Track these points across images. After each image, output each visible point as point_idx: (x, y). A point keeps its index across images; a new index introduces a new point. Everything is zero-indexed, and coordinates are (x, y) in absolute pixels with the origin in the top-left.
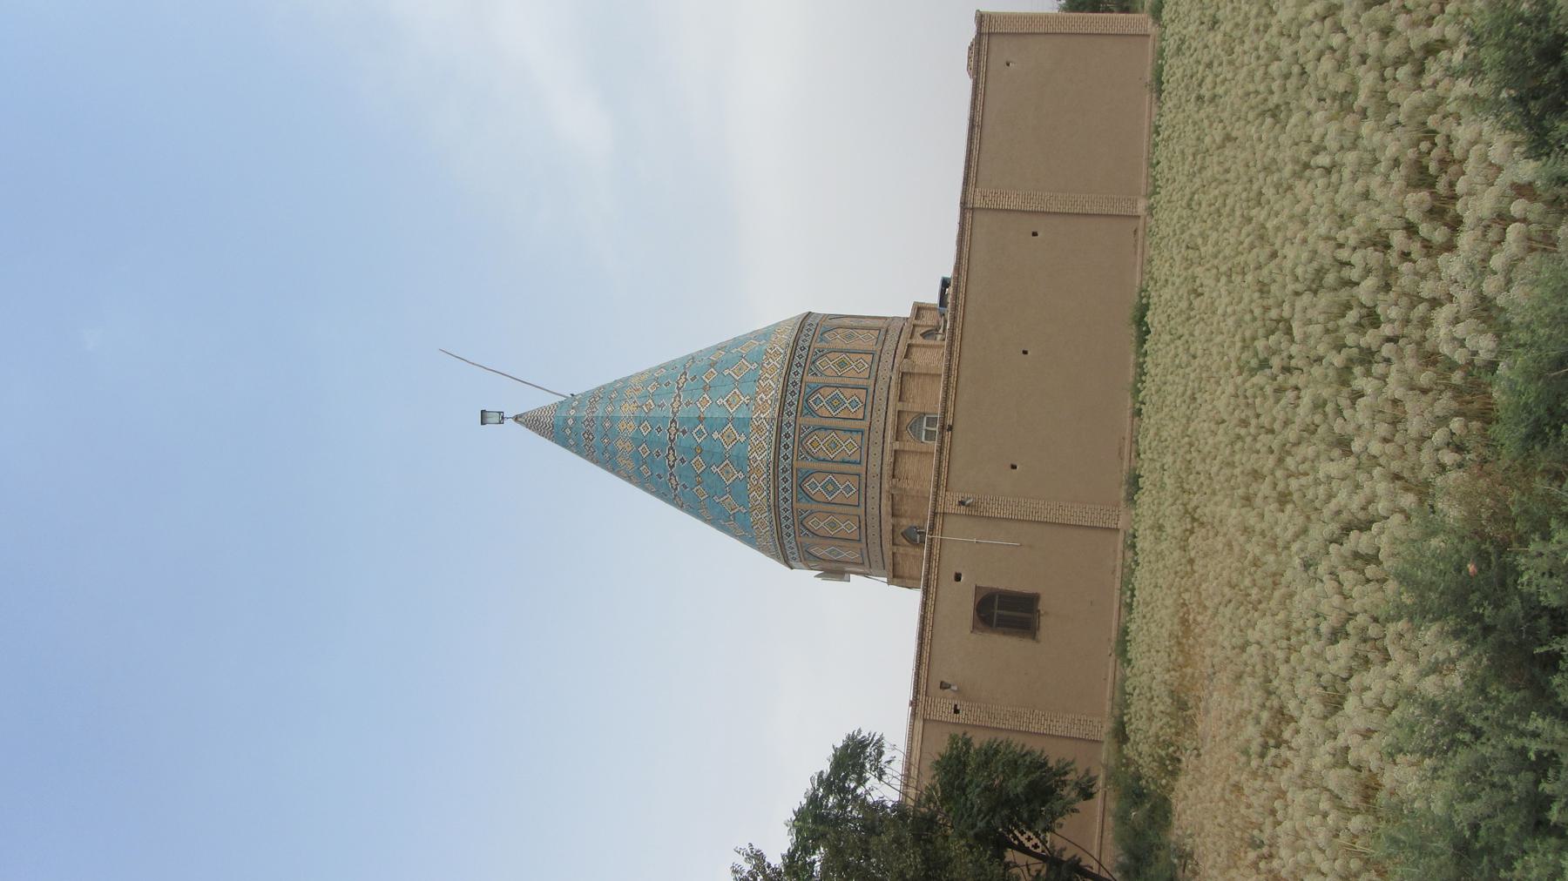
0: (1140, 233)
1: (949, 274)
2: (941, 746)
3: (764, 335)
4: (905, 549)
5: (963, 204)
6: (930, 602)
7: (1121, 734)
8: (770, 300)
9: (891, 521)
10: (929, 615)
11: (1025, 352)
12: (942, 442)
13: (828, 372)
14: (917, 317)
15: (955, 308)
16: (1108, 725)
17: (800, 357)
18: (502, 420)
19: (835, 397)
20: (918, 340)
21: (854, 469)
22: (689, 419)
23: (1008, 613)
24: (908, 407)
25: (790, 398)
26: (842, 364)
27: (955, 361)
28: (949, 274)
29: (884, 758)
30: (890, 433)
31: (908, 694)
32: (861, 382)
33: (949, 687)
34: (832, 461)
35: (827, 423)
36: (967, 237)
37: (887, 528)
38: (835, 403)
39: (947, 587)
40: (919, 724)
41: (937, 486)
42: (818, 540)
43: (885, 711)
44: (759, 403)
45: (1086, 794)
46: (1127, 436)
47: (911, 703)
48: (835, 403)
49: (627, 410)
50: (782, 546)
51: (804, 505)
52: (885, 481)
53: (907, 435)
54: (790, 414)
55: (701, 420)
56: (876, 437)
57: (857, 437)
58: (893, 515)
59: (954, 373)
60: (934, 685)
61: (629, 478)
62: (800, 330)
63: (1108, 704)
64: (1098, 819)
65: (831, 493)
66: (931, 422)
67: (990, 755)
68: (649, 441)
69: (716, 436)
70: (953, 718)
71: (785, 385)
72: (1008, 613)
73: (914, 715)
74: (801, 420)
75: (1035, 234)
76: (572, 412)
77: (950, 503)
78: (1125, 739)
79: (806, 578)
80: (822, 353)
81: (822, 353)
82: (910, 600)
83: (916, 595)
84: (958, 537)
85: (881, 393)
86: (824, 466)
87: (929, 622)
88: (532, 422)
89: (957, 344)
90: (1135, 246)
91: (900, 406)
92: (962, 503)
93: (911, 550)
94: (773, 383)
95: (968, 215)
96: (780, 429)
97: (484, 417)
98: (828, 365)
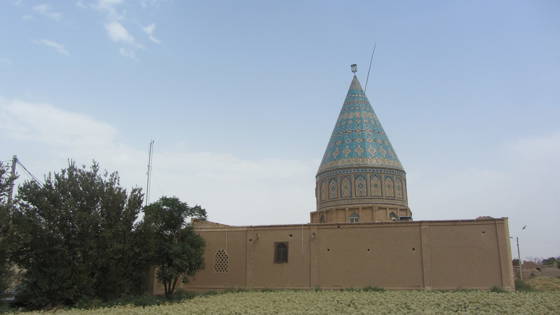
0: (418, 288)
5: (421, 222)
6: (282, 228)
11: (328, 250)
12: (334, 225)
17: (377, 171)
18: (354, 72)
19: (363, 185)
20: (389, 212)
21: (339, 196)
22: (353, 136)
24: (361, 211)
25: (360, 170)
26: (389, 186)
27: (362, 226)
30: (351, 206)
32: (369, 194)
34: (341, 188)
35: (353, 184)
38: (361, 186)
40: (246, 229)
48: (361, 186)
54: (354, 171)
56: (392, 202)
65: (332, 189)
66: (357, 220)
68: (354, 123)
69: (347, 147)
70: (248, 239)
73: (248, 227)
74: (353, 175)
75: (414, 249)
82: (416, 218)
85: (366, 201)
87: (276, 228)
88: (355, 82)
89: (369, 226)
90: (413, 287)
93: (318, 219)
95: (418, 224)
96: (349, 168)
97: (354, 66)
98: (388, 182)
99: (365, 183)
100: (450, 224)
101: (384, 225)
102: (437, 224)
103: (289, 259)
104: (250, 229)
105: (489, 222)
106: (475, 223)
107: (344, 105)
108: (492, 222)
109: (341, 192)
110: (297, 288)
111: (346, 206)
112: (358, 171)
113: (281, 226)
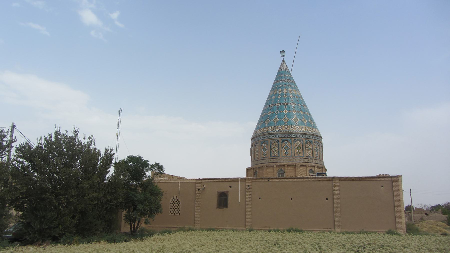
0: (330, 230)
5: (334, 178)
6: (223, 181)
10: (220, 181)
11: (260, 199)
13: (295, 145)
18: (283, 56)
20: (308, 169)
25: (286, 135)
26: (299, 148)
27: (287, 180)
30: (279, 164)
32: (293, 154)
35: (280, 146)
38: (286, 148)
40: (195, 181)
48: (286, 148)
53: (278, 168)
54: (282, 136)
58: (259, 168)
66: (283, 175)
69: (276, 116)
73: (197, 180)
74: (280, 139)
75: (327, 199)
87: (219, 181)
89: (292, 180)
90: (326, 229)
95: (331, 179)
96: (277, 134)
97: (283, 52)
98: (308, 145)
99: (290, 145)
100: (357, 179)
101: (305, 180)
103: (229, 205)
105: (387, 179)
108: (389, 179)
109: (271, 152)
112: (285, 136)
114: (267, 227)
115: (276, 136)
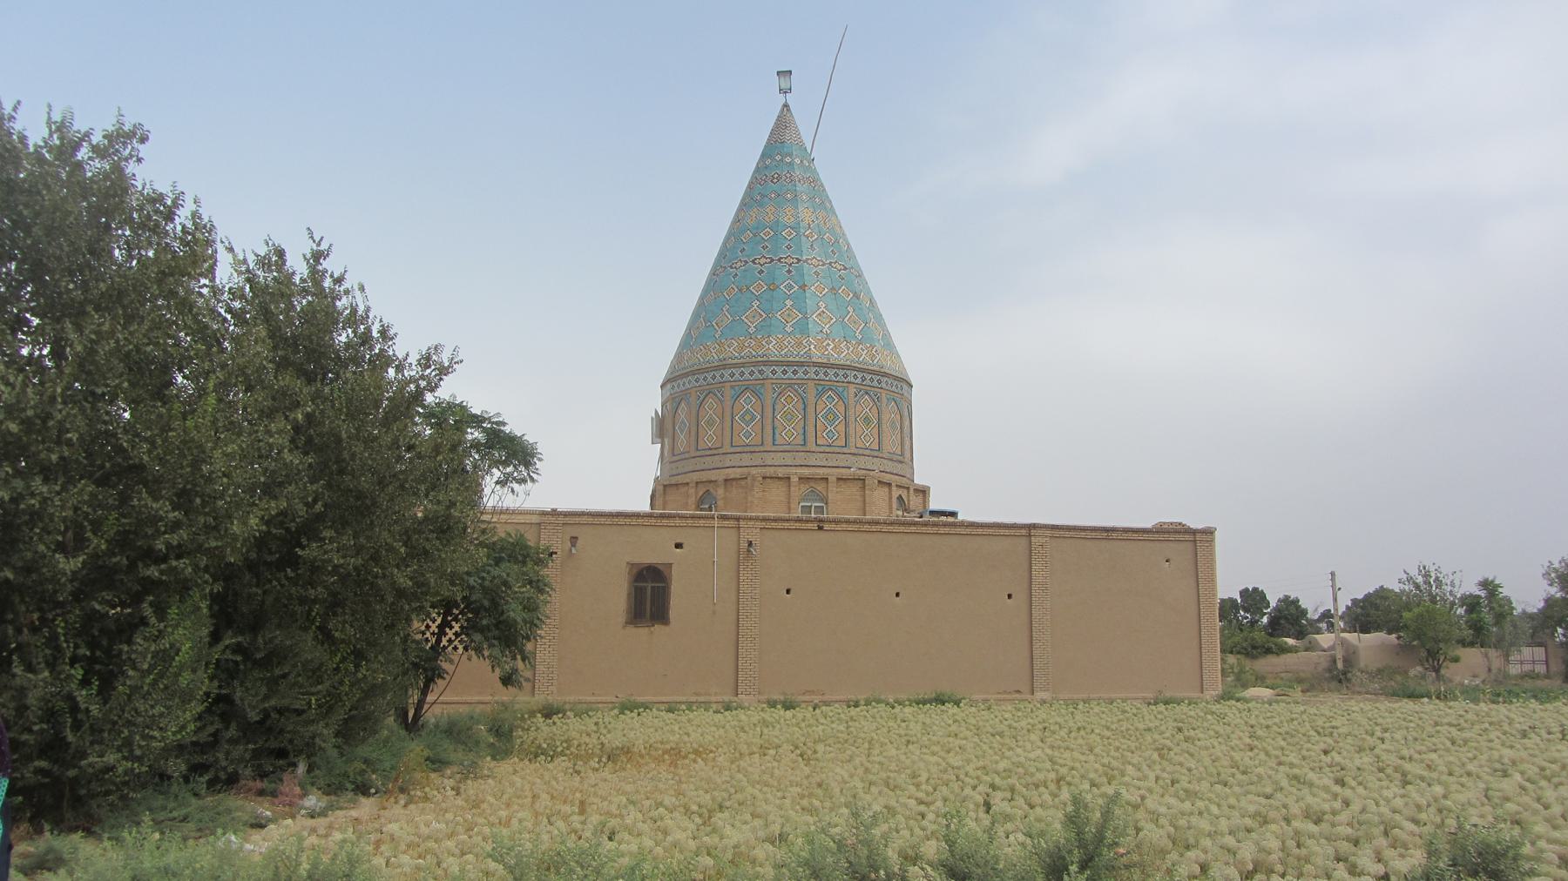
1: (960, 517)
2: (554, 540)
3: (889, 345)
4: (693, 495)
7: (549, 712)
8: (921, 346)
9: (721, 478)
11: (788, 592)
14: (916, 491)
15: (935, 525)
16: (555, 699)
17: (714, 377)
18: (785, 91)
20: (896, 493)
21: (768, 439)
23: (649, 595)
25: (831, 372)
26: (867, 420)
28: (960, 517)
29: (515, 486)
30: (806, 472)
31: (563, 505)
32: (852, 440)
33: (573, 545)
34: (774, 417)
35: (811, 410)
36: (1002, 532)
37: (713, 475)
38: (830, 416)
39: (666, 537)
40: (535, 519)
41: (765, 519)
42: (694, 412)
43: (553, 488)
44: (825, 340)
45: (507, 680)
46: (826, 698)
47: (554, 510)
49: (805, 214)
50: (686, 375)
51: (729, 393)
52: (759, 470)
53: (804, 488)
54: (816, 373)
55: (803, 287)
56: (800, 458)
57: (800, 440)
59: (874, 528)
60: (573, 531)
61: (737, 220)
62: (896, 378)
63: (572, 698)
64: (464, 699)
67: (539, 585)
68: (774, 232)
69: (789, 303)
71: (843, 367)
72: (649, 595)
73: (544, 513)
76: (797, 161)
77: (750, 532)
78: (547, 716)
79: (653, 402)
80: (877, 400)
81: (877, 400)
83: (645, 507)
84: (717, 544)
85: (842, 460)
86: (769, 410)
89: (902, 529)
91: (832, 479)
92: (750, 544)
93: (692, 500)
94: (843, 356)
95: (1024, 532)
96: (801, 364)
98: (865, 406)
100: (1098, 535)
102: (1068, 534)
103: (672, 614)
104: (552, 519)
105: (1180, 537)
106: (1151, 536)
107: (750, 187)
108: (1187, 537)
110: (693, 699)
111: (793, 470)
112: (826, 374)
113: (1126, 530)
114: (812, 692)
115: (795, 373)
